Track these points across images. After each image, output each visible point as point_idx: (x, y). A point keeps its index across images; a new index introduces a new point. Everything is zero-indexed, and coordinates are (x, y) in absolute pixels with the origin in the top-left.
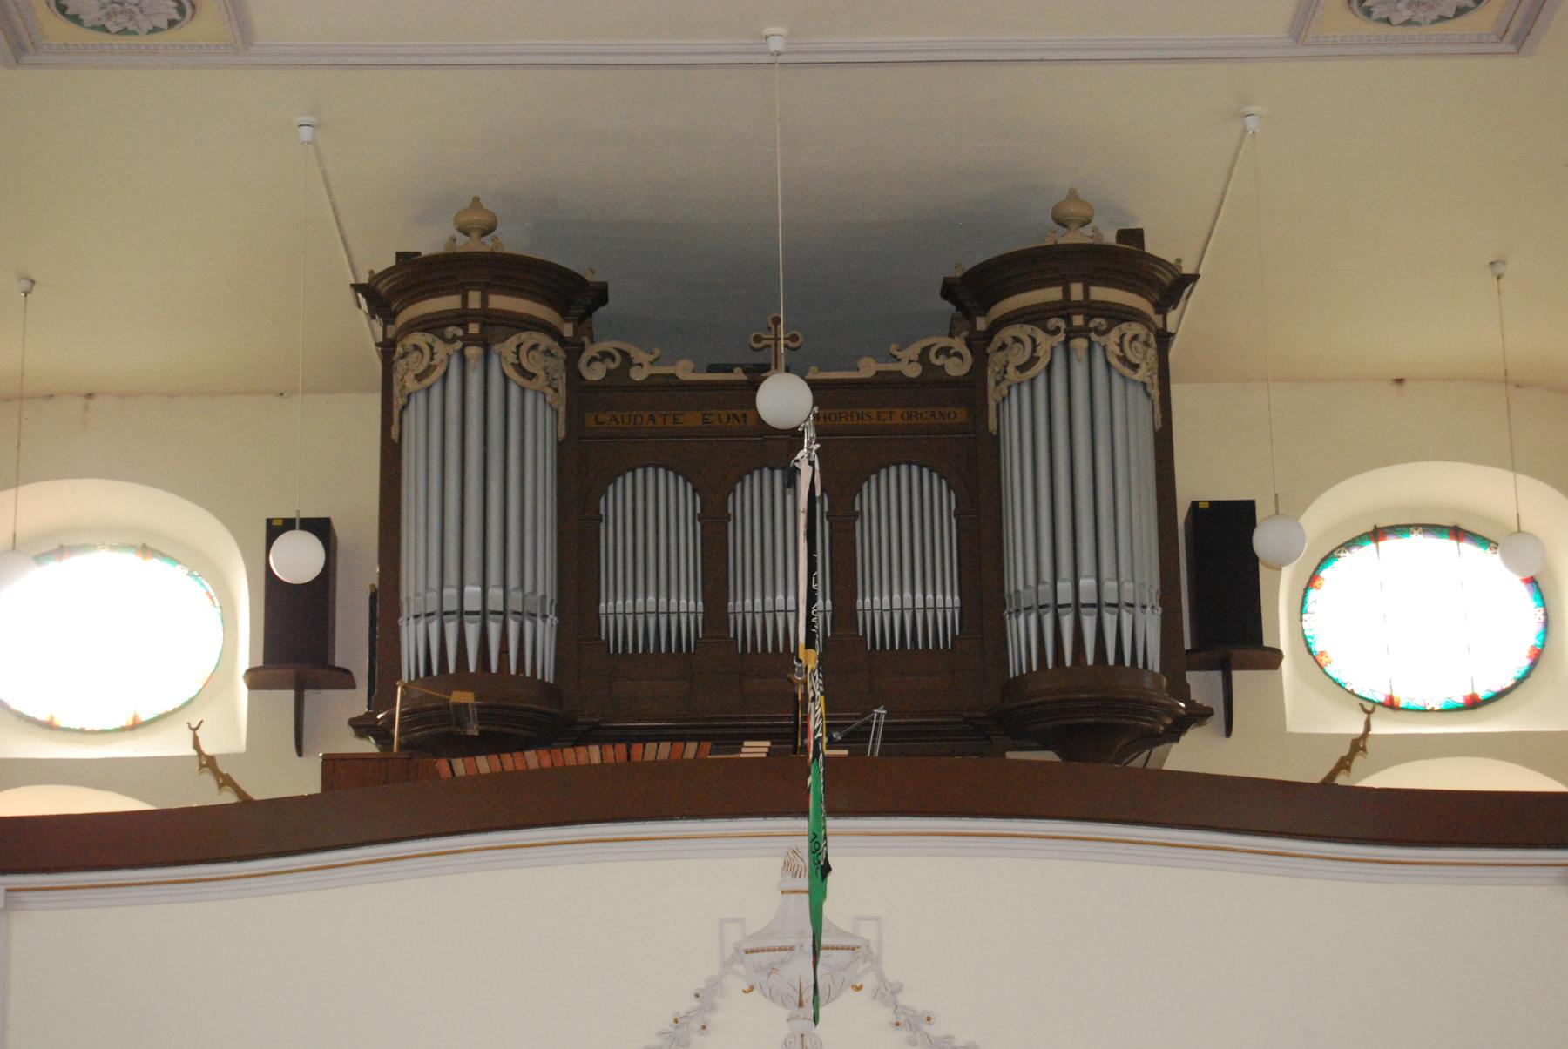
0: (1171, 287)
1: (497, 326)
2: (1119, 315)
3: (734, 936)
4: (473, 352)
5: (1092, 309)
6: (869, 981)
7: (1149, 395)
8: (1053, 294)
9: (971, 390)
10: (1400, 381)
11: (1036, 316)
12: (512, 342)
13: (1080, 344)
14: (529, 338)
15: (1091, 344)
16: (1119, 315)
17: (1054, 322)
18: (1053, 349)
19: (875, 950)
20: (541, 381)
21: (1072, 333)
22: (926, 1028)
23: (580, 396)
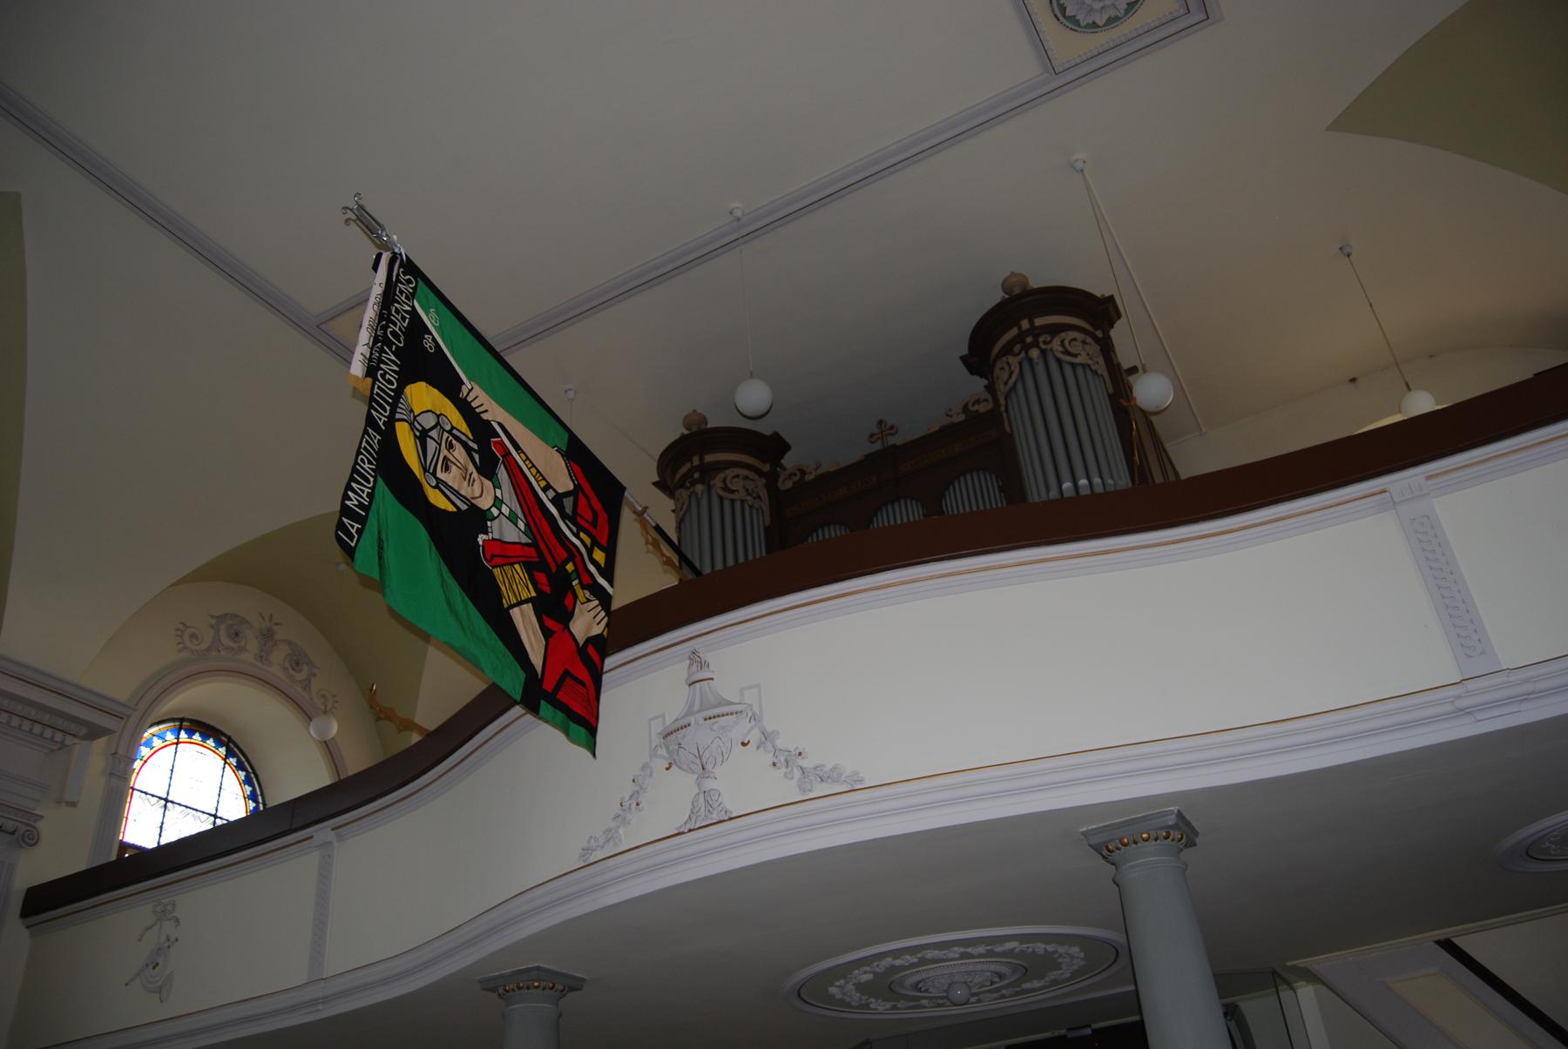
0: (1099, 313)
1: (708, 471)
2: (1055, 330)
3: (658, 727)
4: (699, 488)
5: (1036, 332)
6: (754, 736)
7: (1095, 372)
8: (1014, 332)
9: (994, 418)
10: (1353, 380)
11: (1007, 350)
12: (722, 475)
13: (1034, 353)
14: (730, 473)
15: (1043, 352)
16: (1055, 330)
17: (1017, 348)
18: (1020, 364)
19: (756, 709)
20: (742, 495)
21: (1027, 348)
22: (801, 762)
23: (779, 501)
